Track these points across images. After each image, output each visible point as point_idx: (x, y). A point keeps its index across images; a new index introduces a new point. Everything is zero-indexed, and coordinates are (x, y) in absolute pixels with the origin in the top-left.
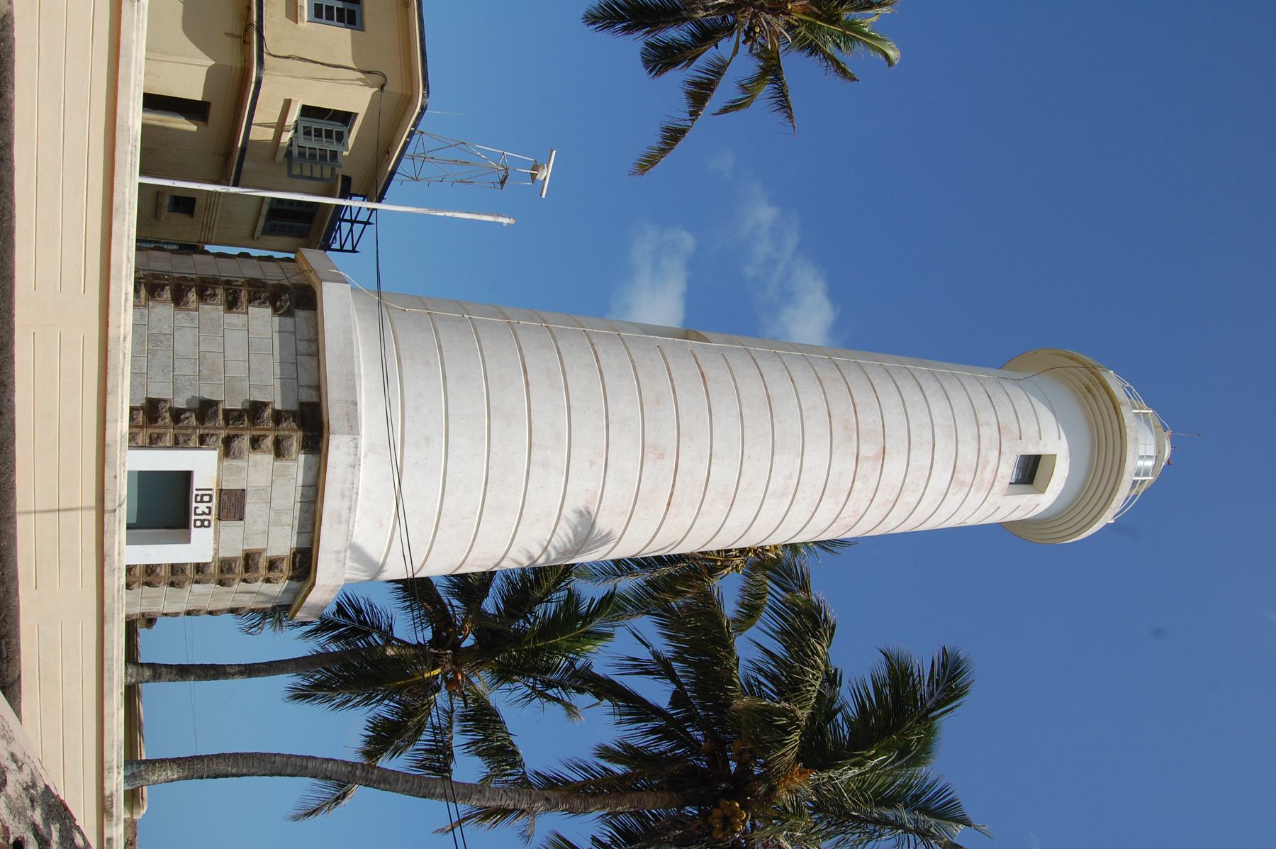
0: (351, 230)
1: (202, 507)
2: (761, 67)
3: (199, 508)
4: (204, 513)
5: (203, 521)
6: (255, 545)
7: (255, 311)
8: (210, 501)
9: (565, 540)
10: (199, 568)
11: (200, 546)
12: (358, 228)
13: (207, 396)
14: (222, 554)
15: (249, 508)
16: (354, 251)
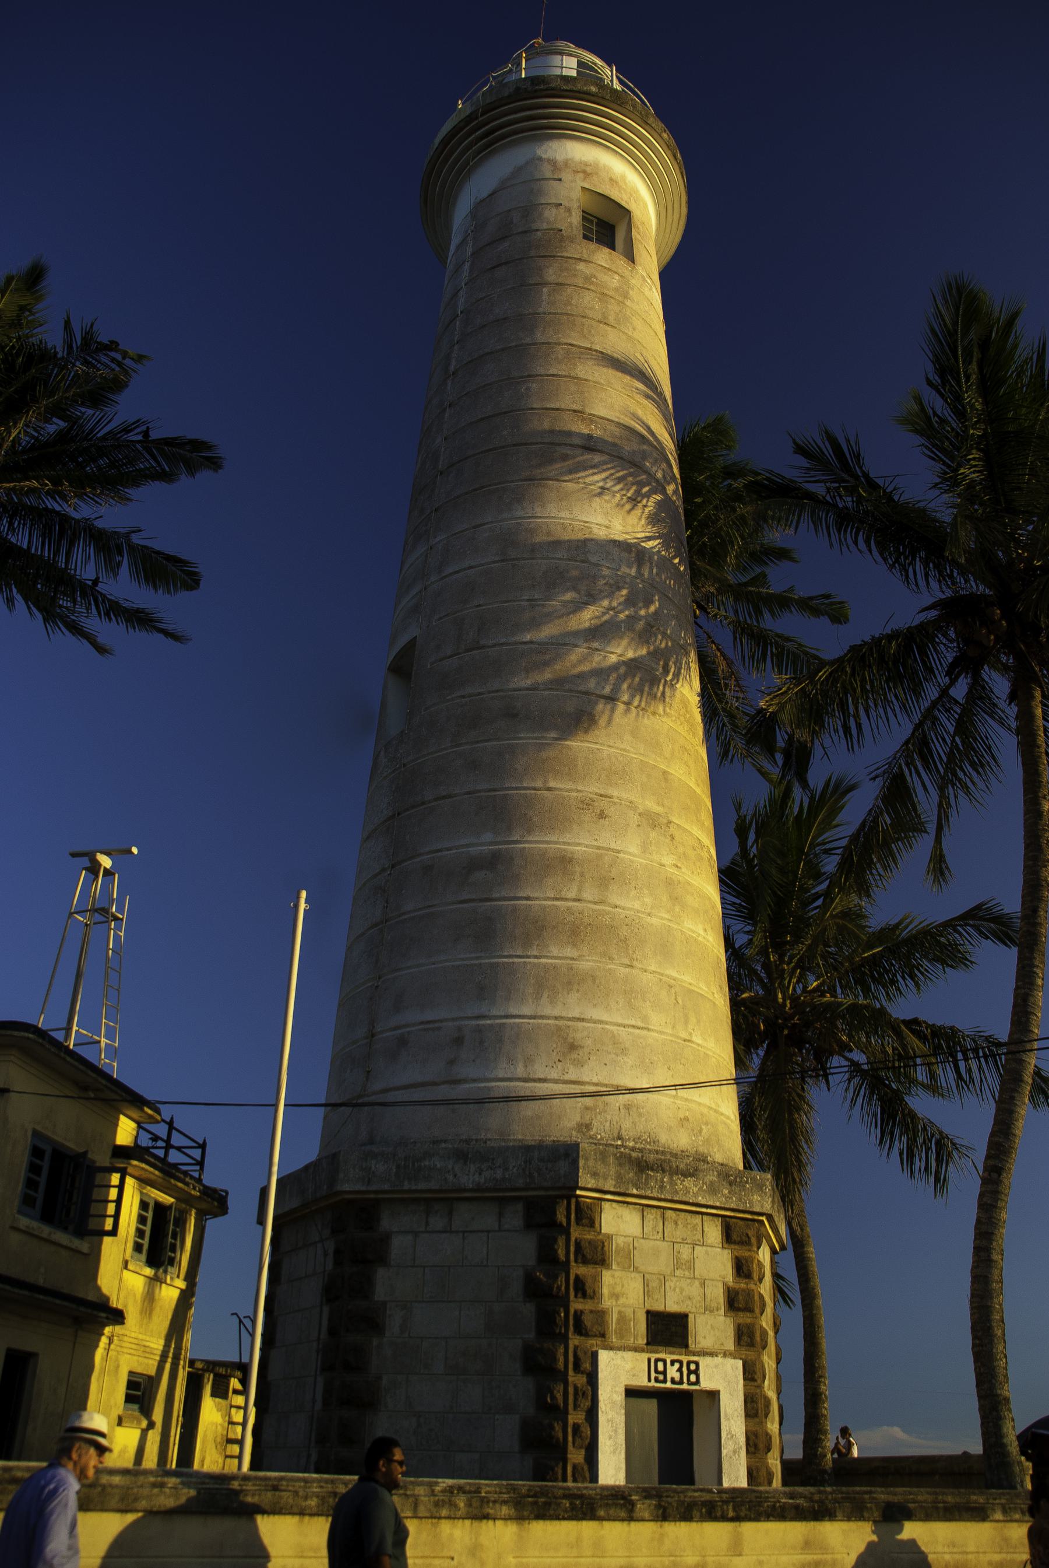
0: (179, 1149)
1: (673, 1372)
4: (680, 1370)
5: (690, 1372)
6: (718, 1295)
7: (380, 1292)
8: (664, 1361)
9: (594, 1073)
11: (721, 1376)
12: (177, 1140)
14: (730, 1345)
15: (673, 1306)
16: (203, 1146)
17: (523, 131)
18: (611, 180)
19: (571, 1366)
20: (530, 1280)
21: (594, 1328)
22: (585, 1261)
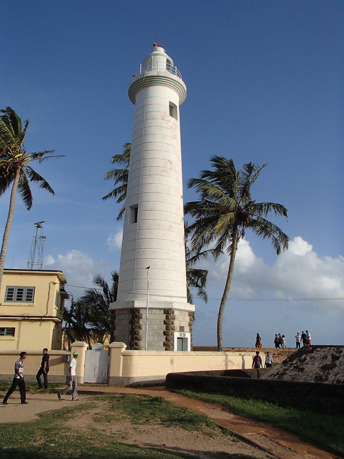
1: (183, 335)
6: (188, 324)
11: (188, 335)
15: (182, 326)
18: (135, 209)
19: (171, 329)
20: (164, 321)
21: (173, 329)
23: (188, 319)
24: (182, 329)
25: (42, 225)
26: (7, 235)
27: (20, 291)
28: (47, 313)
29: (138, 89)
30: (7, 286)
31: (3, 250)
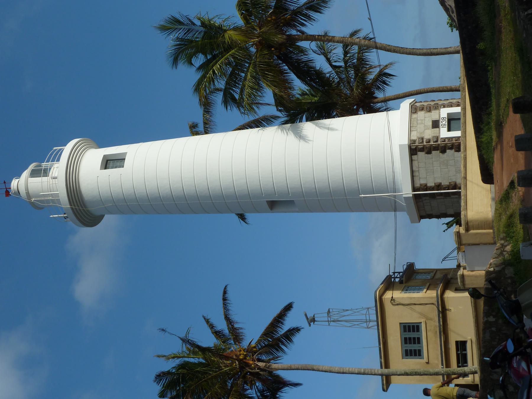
1: (444, 123)
2: (456, 225)
3: (445, 122)
6: (428, 114)
10: (444, 107)
11: (444, 112)
13: (429, 155)
15: (431, 124)
17: (84, 215)
22: (423, 142)
23: (421, 114)
24: (436, 124)
25: (310, 315)
26: (336, 369)
27: (406, 341)
28: (433, 304)
29: (87, 214)
30: (403, 358)
31: (356, 372)
